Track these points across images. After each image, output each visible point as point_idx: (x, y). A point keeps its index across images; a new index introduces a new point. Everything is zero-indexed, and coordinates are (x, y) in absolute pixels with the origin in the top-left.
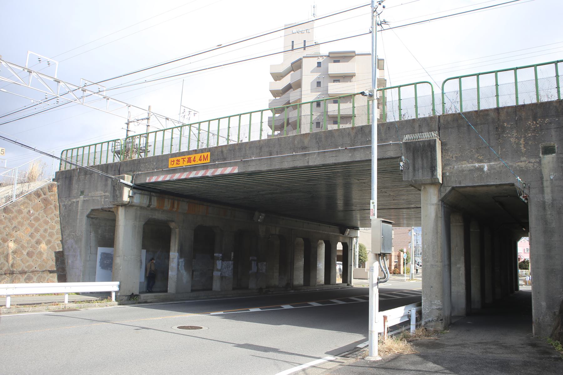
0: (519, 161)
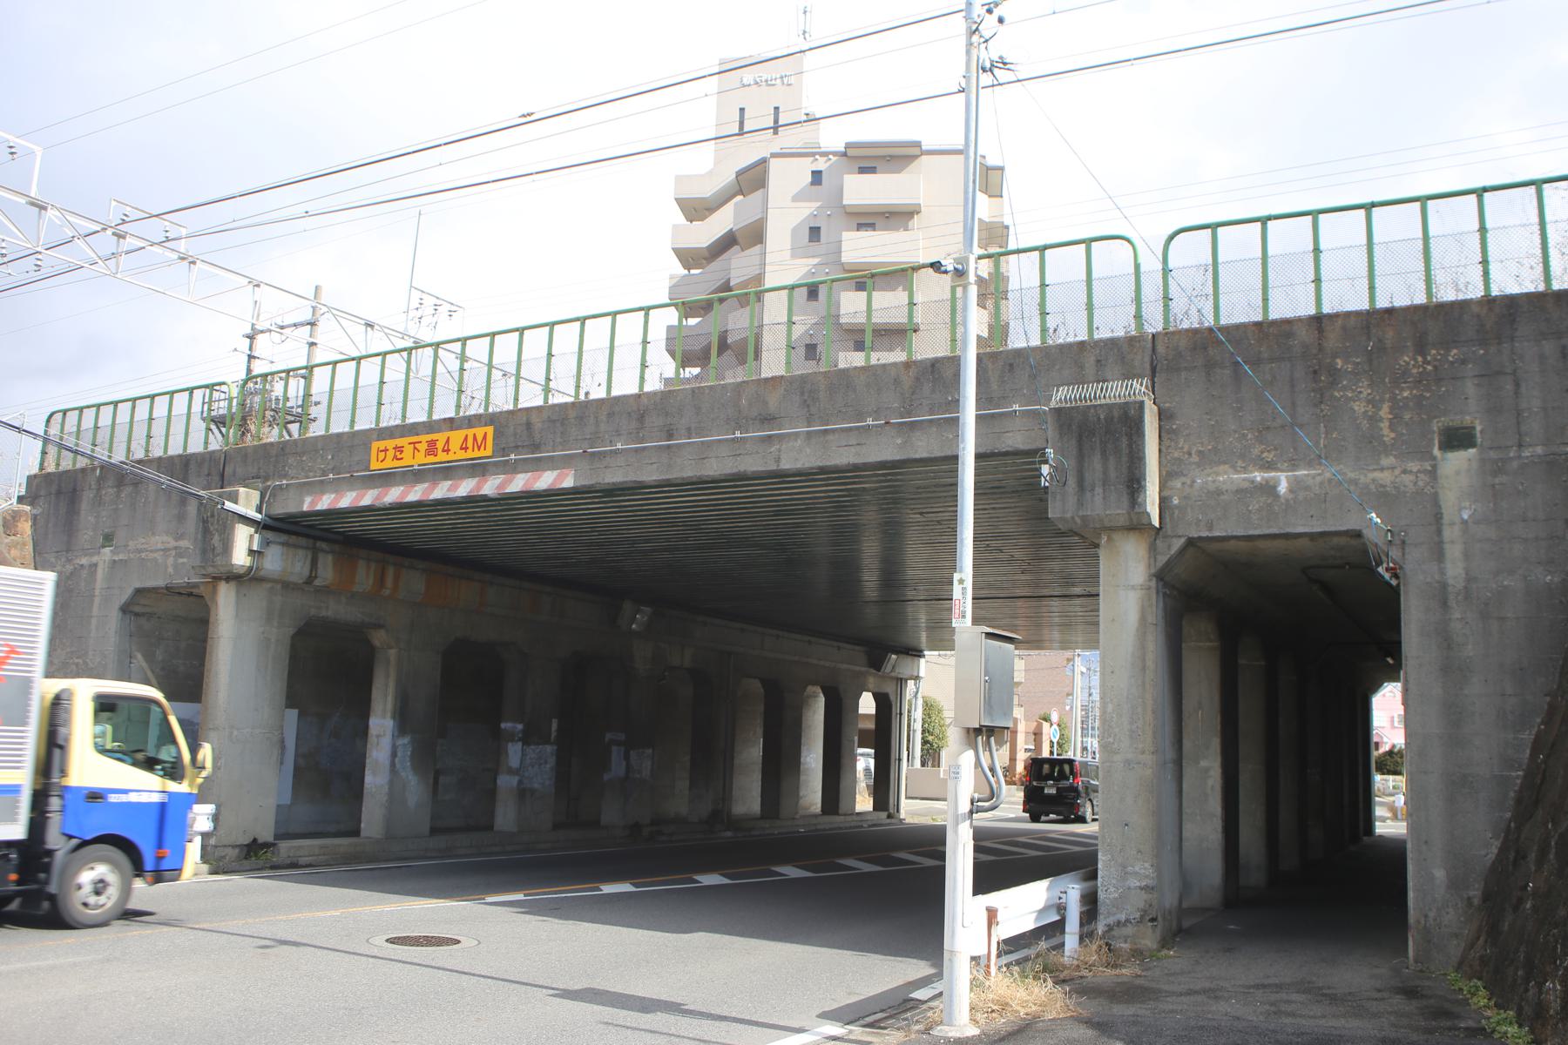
0: (1375, 467)
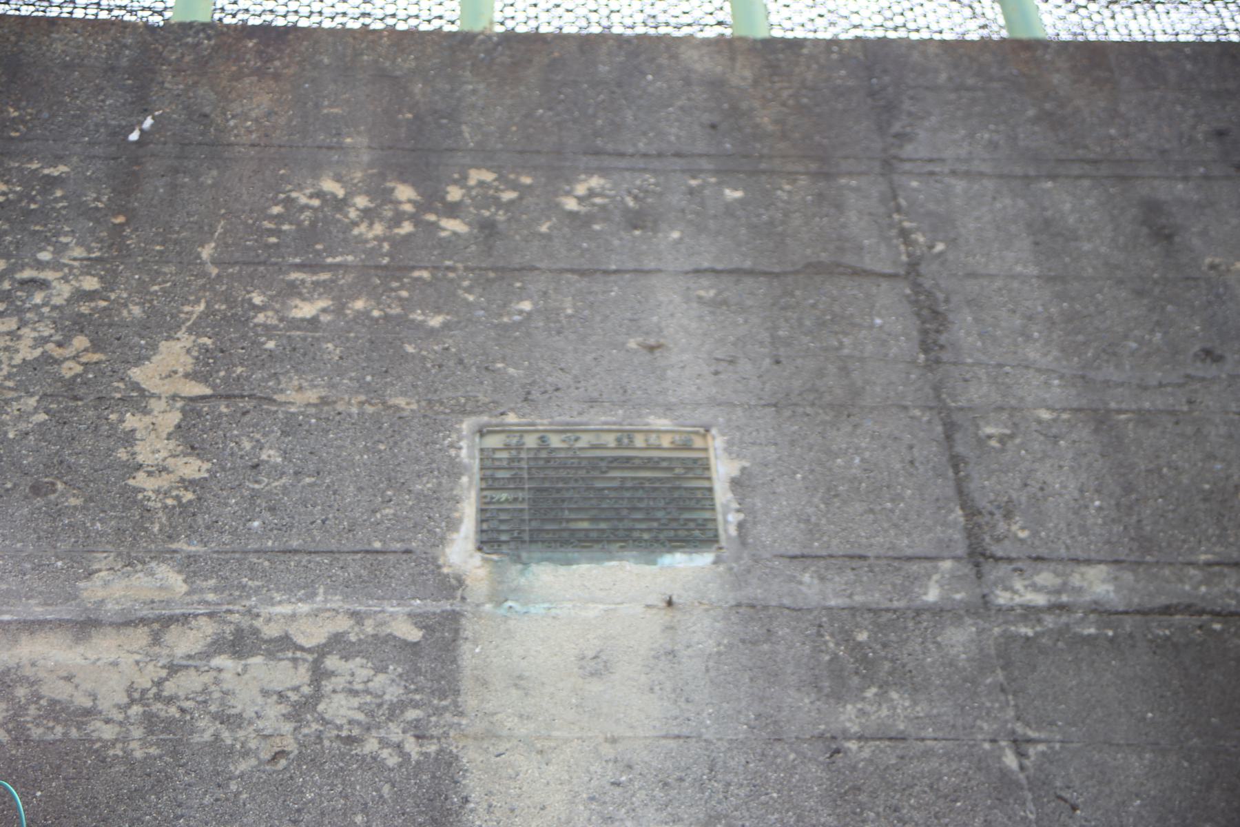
0: (37, 610)
